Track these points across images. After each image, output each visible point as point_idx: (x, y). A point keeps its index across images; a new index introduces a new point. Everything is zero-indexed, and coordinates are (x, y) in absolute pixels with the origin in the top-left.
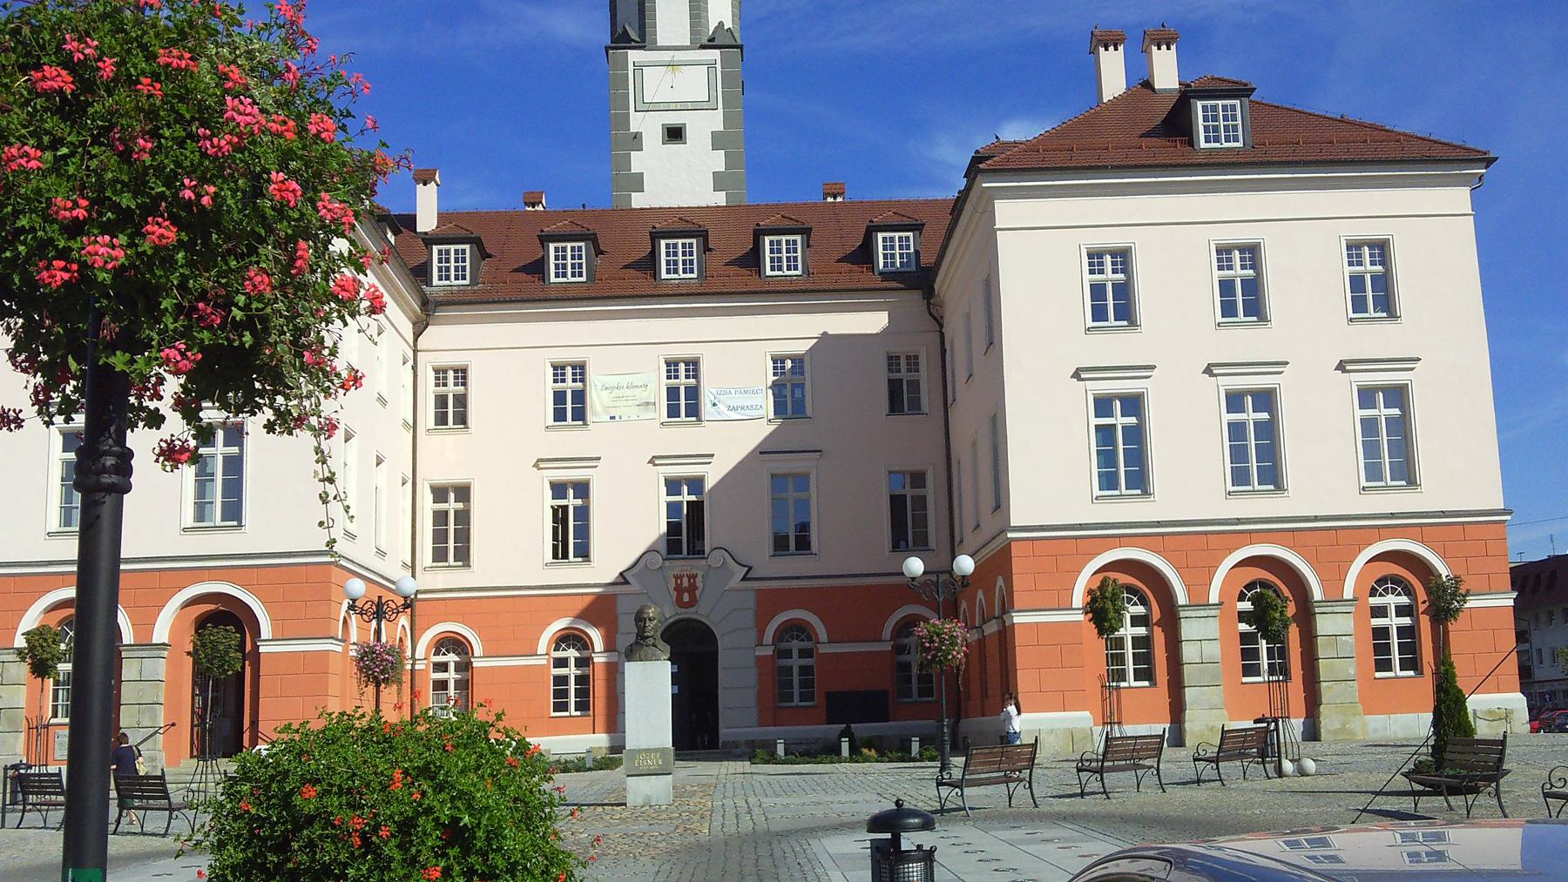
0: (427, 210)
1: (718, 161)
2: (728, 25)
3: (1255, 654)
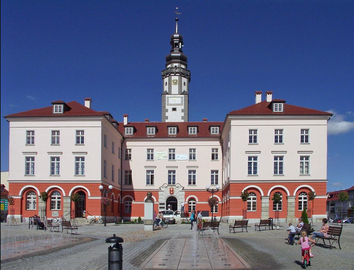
2: (186, 90)
3: (276, 206)
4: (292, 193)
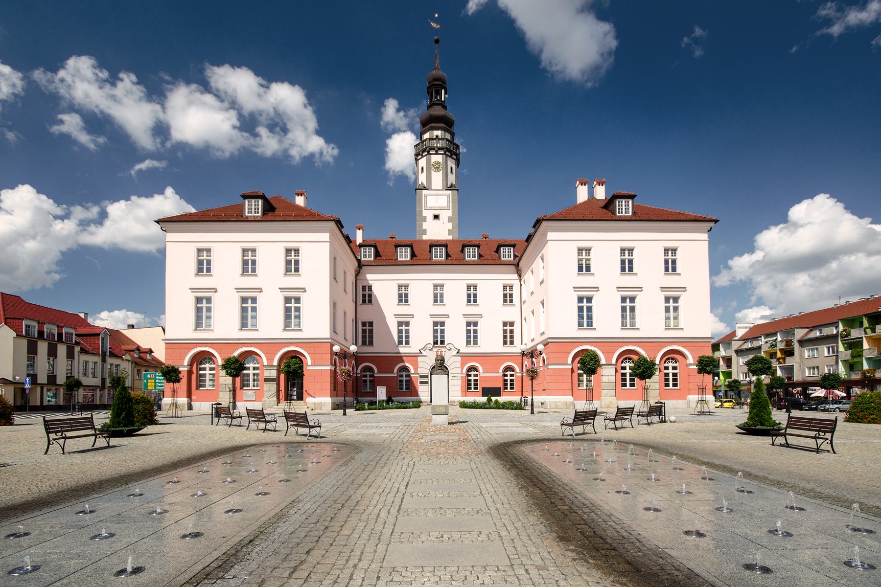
0: (359, 238)
1: (450, 226)
4: (609, 358)
